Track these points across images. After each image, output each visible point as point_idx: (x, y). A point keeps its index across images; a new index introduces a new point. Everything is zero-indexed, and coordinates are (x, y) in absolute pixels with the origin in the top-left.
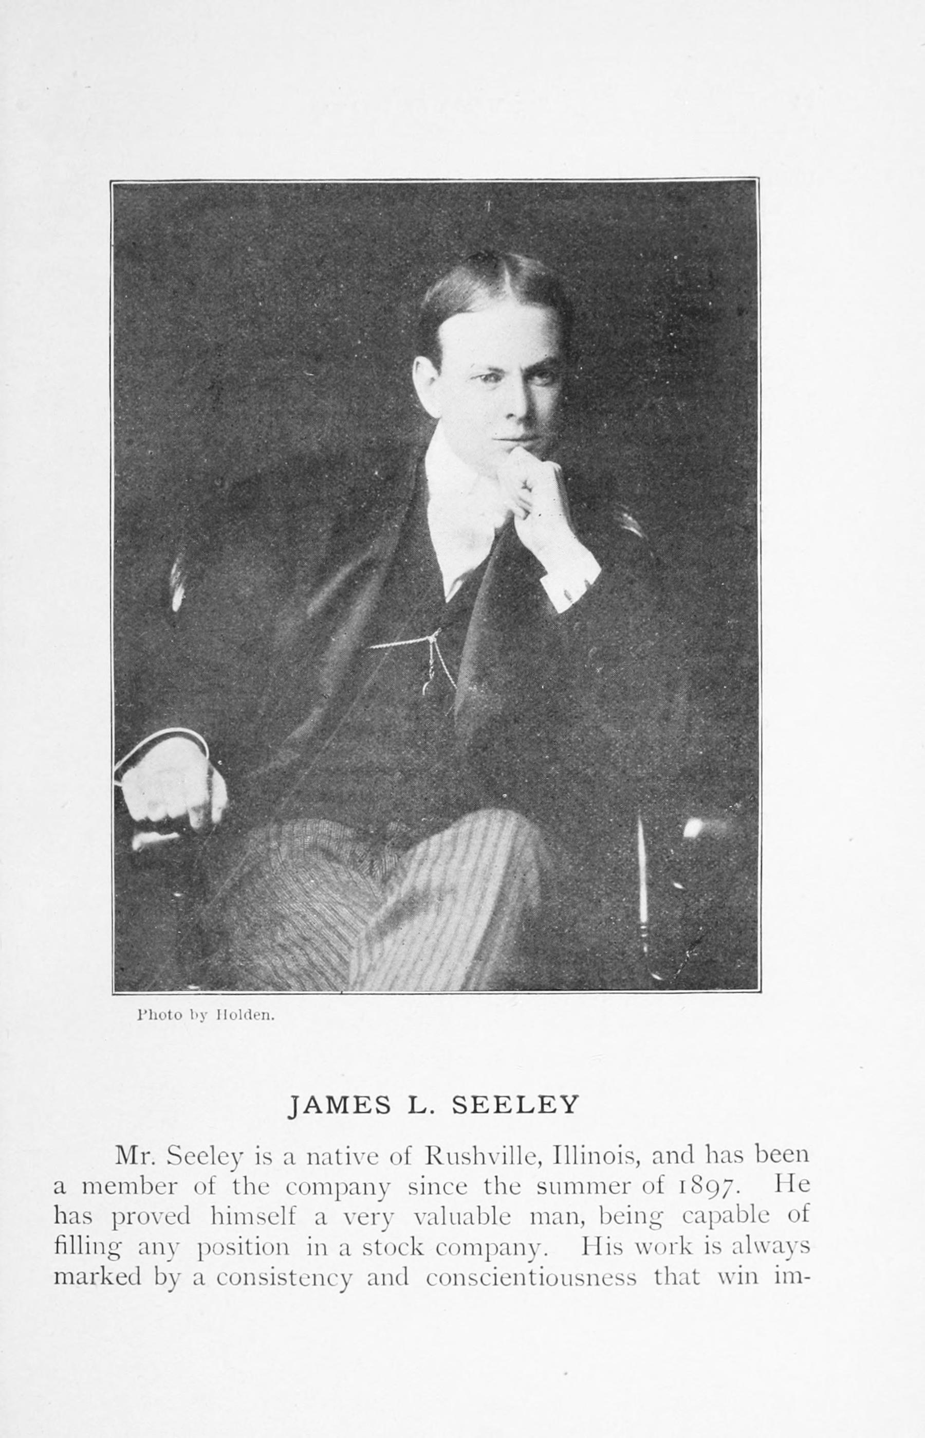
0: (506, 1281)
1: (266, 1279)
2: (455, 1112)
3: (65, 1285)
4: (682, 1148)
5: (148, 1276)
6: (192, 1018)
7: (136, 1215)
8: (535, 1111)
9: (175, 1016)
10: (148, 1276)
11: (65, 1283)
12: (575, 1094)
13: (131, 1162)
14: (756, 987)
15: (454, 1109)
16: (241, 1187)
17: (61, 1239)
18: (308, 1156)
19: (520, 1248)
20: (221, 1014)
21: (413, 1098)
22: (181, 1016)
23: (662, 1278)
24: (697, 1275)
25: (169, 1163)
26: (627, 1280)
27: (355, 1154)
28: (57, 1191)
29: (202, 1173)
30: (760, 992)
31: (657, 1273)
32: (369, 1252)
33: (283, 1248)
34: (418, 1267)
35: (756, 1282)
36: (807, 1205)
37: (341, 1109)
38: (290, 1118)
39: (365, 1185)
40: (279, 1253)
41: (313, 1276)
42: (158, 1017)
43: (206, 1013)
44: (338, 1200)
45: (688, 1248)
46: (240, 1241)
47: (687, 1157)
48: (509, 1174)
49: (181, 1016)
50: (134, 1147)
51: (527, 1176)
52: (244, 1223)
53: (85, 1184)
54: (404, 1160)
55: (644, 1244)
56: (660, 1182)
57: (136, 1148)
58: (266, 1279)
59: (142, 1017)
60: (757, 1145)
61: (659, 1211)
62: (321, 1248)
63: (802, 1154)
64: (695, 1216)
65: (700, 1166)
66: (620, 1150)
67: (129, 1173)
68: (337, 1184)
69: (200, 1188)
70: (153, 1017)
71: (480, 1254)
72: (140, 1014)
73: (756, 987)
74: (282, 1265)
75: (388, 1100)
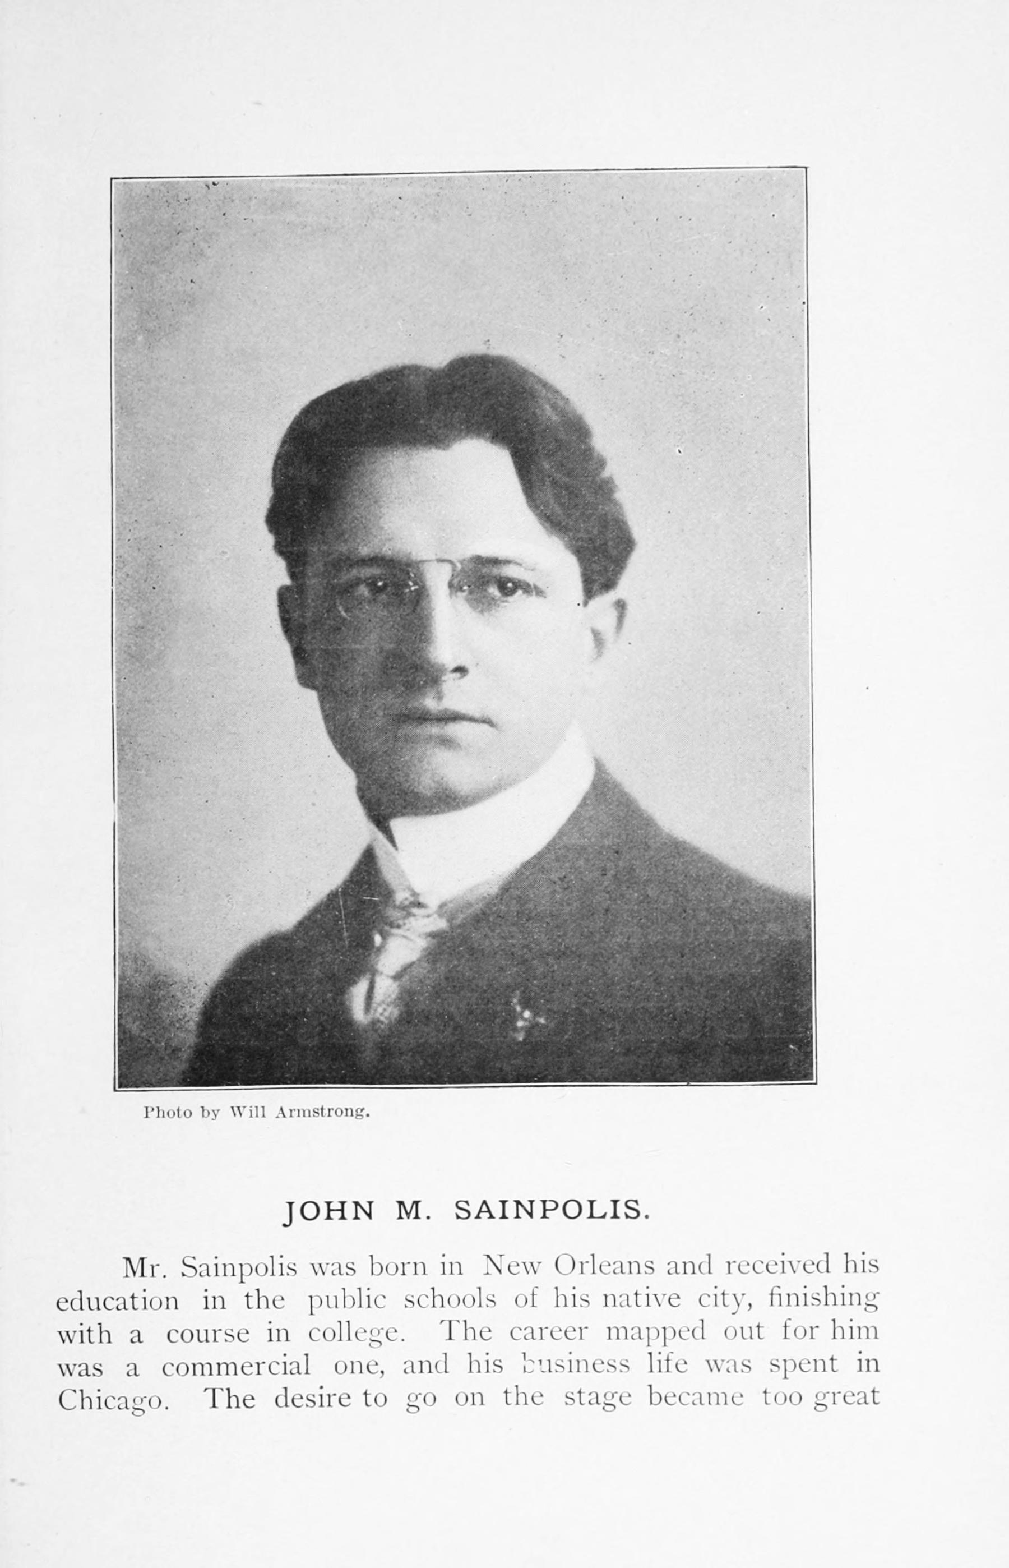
0: (297, 1402)
2: (458, 1217)
3: (321, 1408)
4: (700, 1258)
6: (203, 1116)
7: (549, 1331)
14: (812, 1079)
16: (253, 1301)
17: (776, 1291)
18: (727, 1264)
22: (191, 1113)
23: (512, 1398)
24: (876, 1394)
25: (183, 1275)
26: (619, 1367)
27: (790, 1262)
29: (524, 1283)
30: (816, 1084)
31: (366, 1394)
32: (562, 1369)
33: (478, 1398)
36: (788, 1322)
37: (413, 1214)
38: (285, 1225)
42: (344, 1111)
44: (312, 1314)
47: (705, 1268)
48: (271, 1285)
49: (191, 1113)
50: (142, 1259)
52: (868, 1338)
54: (400, 1271)
55: (320, 1265)
56: (533, 1295)
57: (145, 1260)
59: (149, 1115)
61: (379, 1328)
62: (283, 1334)
63: (420, 1267)
64: (524, 1333)
65: (721, 1279)
66: (863, 1257)
67: (135, 1285)
69: (521, 1301)
72: (147, 1112)
73: (812, 1079)
74: (572, 1382)
75: (468, 1204)
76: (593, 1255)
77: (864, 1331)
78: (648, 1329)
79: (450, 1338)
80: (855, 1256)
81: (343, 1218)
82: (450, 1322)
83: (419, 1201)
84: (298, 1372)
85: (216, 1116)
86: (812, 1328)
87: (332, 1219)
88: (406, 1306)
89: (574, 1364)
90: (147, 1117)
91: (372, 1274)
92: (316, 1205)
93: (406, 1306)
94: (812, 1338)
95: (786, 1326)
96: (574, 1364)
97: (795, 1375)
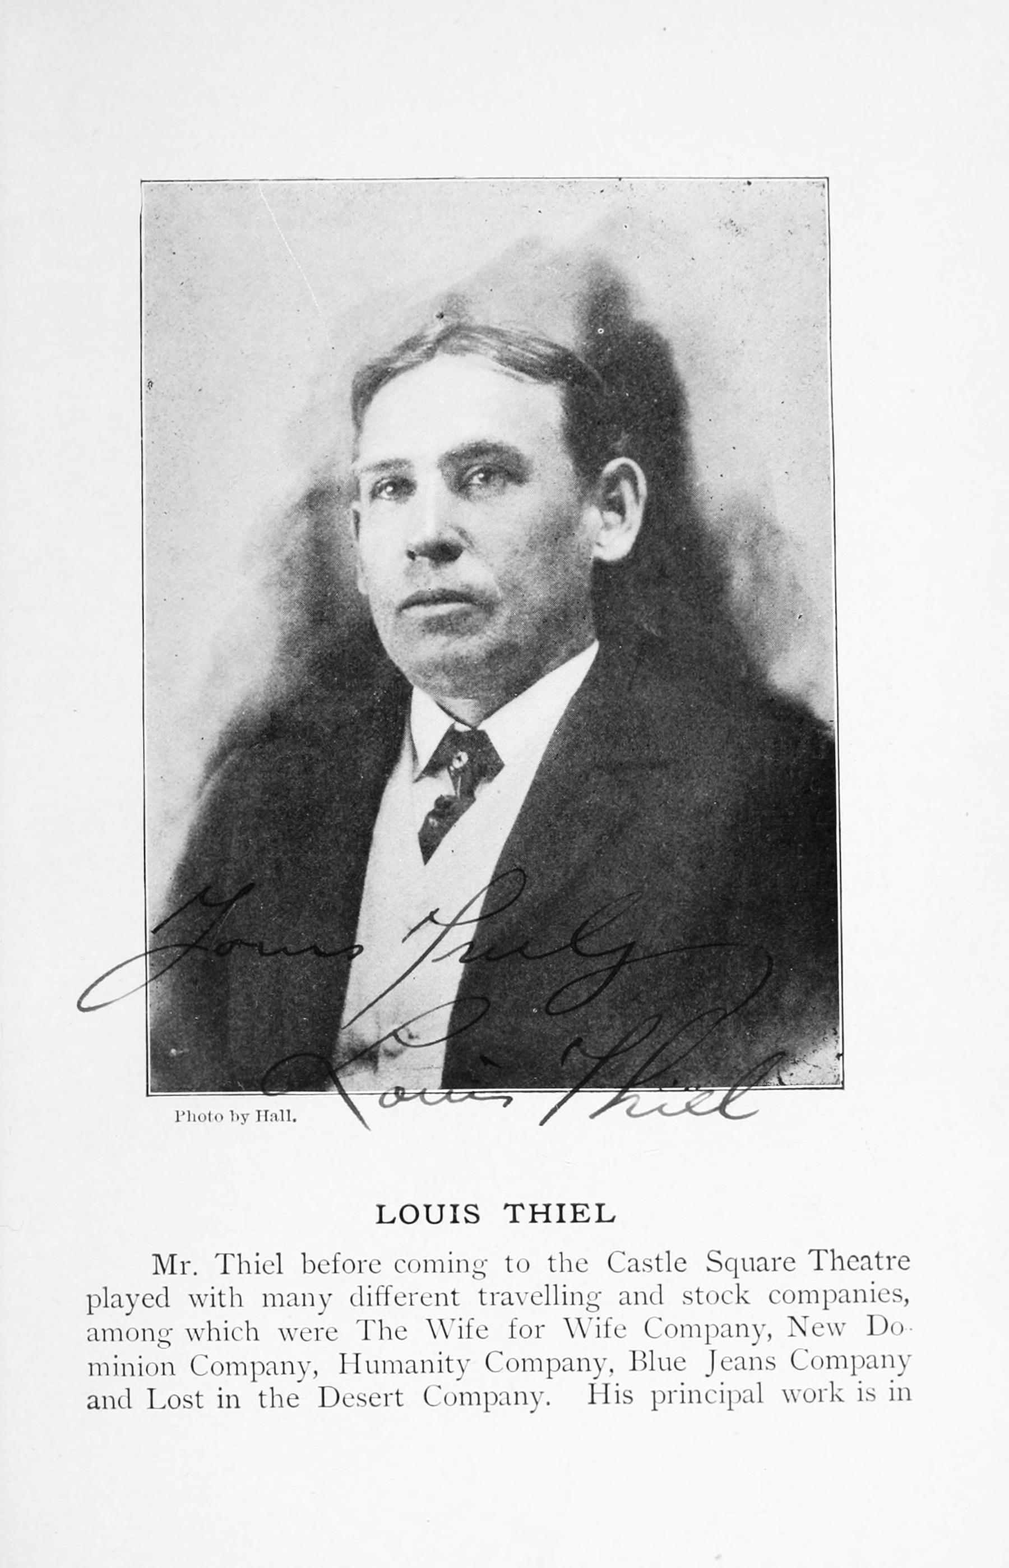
1: (190, 1402)
4: (268, 1256)
5: (210, 1400)
6: (232, 1120)
8: (590, 1221)
9: (216, 1118)
10: (210, 1400)
11: (229, 1407)
12: (533, 1203)
13: (170, 1272)
14: (152, 1091)
15: (466, 1219)
19: (288, 1367)
20: (263, 1115)
21: (381, 1207)
22: (222, 1118)
25: (709, 1270)
28: (505, 1302)
30: (148, 1095)
33: (168, 1367)
34: (774, 1382)
35: (909, 1399)
36: (515, 1321)
39: (636, 1294)
40: (164, 1374)
41: (384, 1397)
43: (248, 1114)
45: (745, 1297)
46: (440, 1357)
49: (222, 1118)
51: (675, 1284)
53: (265, 1296)
55: (289, 1330)
57: (175, 1257)
58: (190, 1402)
60: (304, 1254)
62: (233, 1400)
68: (825, 1292)
70: (192, 1118)
71: (245, 1374)
76: (279, 1254)
77: (389, 1365)
78: (707, 1326)
79: (366, 1338)
80: (249, 1256)
81: (547, 1221)
82: (366, 1321)
83: (458, 1205)
84: (743, 1368)
85: (245, 1120)
86: (538, 1327)
87: (536, 1222)
88: (684, 1303)
89: (120, 1368)
90: (178, 1121)
91: (305, 1272)
92: (413, 1206)
93: (684, 1303)
94: (538, 1337)
95: (512, 1326)
96: (120, 1368)
97: (862, 1372)
